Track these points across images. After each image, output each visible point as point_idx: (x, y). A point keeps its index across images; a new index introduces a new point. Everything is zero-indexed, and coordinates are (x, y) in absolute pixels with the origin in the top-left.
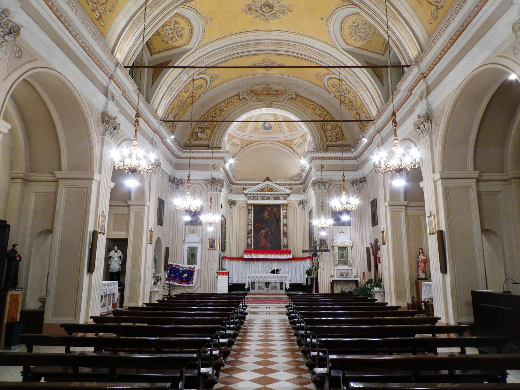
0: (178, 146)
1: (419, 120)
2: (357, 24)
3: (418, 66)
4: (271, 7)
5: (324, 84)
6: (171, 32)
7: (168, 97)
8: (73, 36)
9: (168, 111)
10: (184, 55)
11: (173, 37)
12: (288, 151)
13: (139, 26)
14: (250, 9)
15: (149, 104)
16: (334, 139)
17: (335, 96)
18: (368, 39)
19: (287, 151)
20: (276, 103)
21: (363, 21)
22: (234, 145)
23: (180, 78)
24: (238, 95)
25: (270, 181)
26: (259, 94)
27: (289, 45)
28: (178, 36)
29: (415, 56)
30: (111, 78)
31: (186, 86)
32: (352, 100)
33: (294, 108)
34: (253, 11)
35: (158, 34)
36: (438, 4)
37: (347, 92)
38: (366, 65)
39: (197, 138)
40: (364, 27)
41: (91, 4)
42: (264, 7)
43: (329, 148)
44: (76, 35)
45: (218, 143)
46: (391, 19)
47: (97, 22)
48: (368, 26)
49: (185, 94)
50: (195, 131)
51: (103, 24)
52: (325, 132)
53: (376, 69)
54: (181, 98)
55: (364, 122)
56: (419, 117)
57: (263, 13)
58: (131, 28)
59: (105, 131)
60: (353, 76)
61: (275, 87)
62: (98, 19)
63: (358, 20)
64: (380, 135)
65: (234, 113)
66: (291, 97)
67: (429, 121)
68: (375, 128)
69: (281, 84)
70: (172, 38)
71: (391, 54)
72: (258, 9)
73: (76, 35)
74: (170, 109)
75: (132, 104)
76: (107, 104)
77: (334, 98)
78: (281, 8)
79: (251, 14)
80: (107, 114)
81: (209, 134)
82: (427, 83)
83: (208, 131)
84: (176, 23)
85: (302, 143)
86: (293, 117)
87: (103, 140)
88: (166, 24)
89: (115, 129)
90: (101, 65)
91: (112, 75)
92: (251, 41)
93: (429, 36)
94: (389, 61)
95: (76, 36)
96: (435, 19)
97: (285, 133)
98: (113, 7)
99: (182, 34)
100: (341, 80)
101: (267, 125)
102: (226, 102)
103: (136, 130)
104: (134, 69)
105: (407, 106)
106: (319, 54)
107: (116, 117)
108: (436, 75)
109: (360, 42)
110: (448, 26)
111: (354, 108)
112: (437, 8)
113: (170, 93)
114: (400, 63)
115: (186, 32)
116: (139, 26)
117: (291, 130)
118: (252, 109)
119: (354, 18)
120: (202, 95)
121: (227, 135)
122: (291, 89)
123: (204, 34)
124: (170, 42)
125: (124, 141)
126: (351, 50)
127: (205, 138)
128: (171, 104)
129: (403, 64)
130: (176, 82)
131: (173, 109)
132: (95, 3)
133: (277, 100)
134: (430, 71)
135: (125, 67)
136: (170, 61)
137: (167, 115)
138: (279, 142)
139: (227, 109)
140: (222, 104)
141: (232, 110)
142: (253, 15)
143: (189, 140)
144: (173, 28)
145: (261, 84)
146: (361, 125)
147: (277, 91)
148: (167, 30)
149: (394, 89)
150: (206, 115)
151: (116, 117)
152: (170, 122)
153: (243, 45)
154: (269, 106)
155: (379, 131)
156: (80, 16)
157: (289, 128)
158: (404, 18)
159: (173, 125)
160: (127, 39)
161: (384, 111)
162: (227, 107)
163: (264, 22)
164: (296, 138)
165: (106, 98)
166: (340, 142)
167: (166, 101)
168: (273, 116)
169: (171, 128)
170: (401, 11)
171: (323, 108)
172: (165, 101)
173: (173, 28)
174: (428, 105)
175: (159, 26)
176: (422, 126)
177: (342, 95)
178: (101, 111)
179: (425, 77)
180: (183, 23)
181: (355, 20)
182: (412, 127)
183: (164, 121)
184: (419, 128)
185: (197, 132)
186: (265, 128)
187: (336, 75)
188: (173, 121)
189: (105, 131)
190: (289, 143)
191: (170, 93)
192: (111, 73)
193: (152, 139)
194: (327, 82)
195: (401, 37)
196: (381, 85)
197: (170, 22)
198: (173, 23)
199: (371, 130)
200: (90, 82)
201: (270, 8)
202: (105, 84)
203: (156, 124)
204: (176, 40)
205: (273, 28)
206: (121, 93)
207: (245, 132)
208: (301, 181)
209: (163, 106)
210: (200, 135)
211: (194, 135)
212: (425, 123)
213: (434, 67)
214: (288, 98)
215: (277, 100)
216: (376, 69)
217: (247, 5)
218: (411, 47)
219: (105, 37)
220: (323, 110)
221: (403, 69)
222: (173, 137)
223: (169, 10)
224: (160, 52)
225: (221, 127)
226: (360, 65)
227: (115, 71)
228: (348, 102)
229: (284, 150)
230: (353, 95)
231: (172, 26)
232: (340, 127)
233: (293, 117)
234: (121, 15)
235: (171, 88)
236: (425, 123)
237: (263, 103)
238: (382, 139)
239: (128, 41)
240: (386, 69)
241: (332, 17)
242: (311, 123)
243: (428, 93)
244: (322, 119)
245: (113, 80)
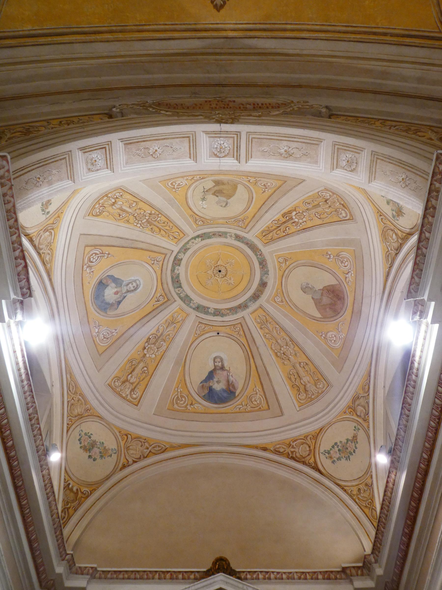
12: (300, 478)
19: (297, 479)
25: (231, 572)
85: (355, 439)
138: (265, 449)
190: (302, 451)
207: (137, 403)
208: (379, 571)
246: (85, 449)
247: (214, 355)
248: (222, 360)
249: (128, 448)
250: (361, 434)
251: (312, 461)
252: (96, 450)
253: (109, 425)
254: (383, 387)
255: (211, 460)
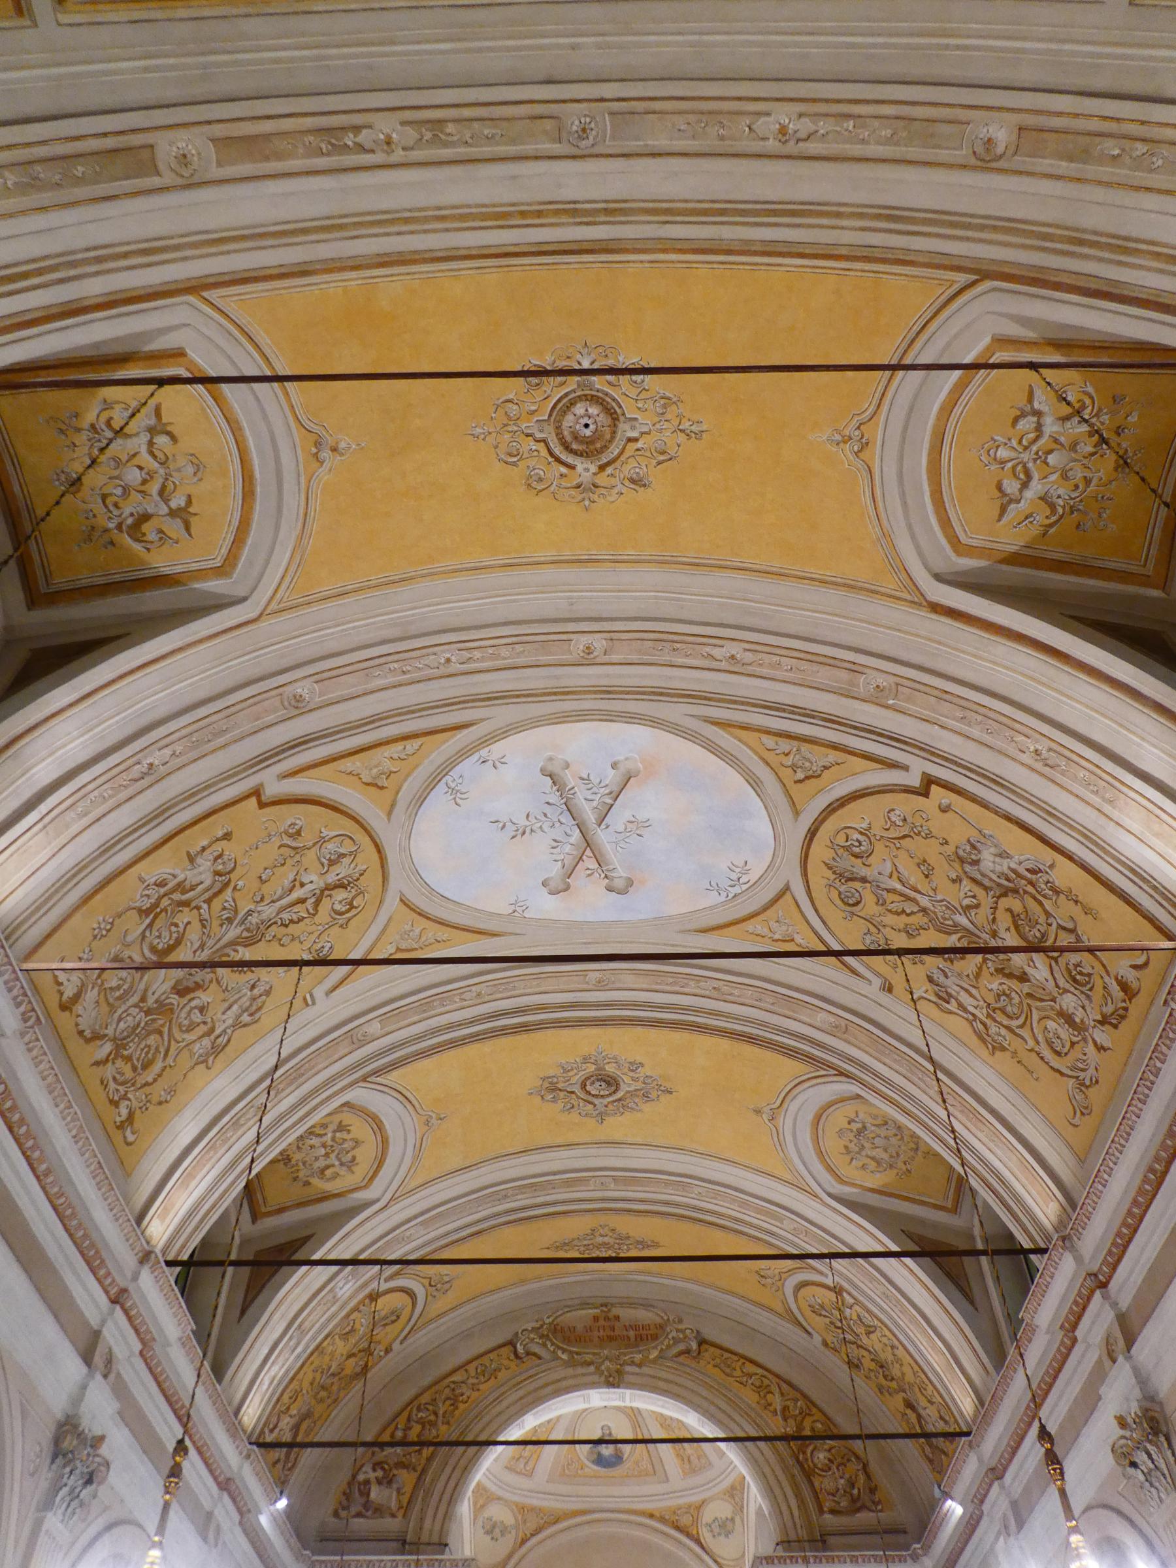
0: (293, 1540)
1: (1127, 1434)
2: (860, 1125)
3: (1073, 1249)
4: (611, 1082)
5: (784, 1302)
6: (323, 1151)
7: (286, 1354)
8: (38, 1177)
9: (277, 1408)
10: (352, 1218)
11: (327, 1167)
13: (232, 1141)
14: (554, 1088)
15: (220, 1381)
16: (844, 1504)
17: (825, 1344)
18: (900, 1165)
20: (637, 1370)
21: (875, 1117)
22: (492, 1530)
23: (331, 1290)
24: (511, 1343)
26: (579, 1340)
27: (667, 1183)
28: (342, 1164)
29: (1054, 1219)
30: (118, 1299)
31: (348, 1315)
32: (882, 1356)
33: (695, 1387)
34: (562, 1094)
35: (284, 1158)
36: (1082, 1075)
37: (861, 1330)
38: (913, 1247)
39: (367, 1505)
40: (883, 1132)
41: (112, 1086)
42: (593, 1083)
43: (832, 1540)
44: (48, 1172)
45: (437, 1527)
46: (959, 1116)
47: (117, 1137)
48: (894, 1131)
49: (340, 1344)
50: (361, 1477)
51: (131, 1138)
52: (808, 1475)
53: (944, 1260)
54: (327, 1358)
55: (942, 1440)
56: (1122, 1422)
57: (590, 1098)
58: (212, 1147)
59: (55, 1488)
60: (873, 1279)
61: (628, 1315)
62: (121, 1127)
63: (861, 1115)
64: (1002, 1487)
65: (498, 1409)
66: (681, 1347)
67: (1162, 1439)
68: (980, 1460)
69: (647, 1305)
70: (322, 1171)
71: (980, 1210)
72: (577, 1089)
73: (48, 1172)
74: (286, 1397)
75: (165, 1385)
76: (84, 1387)
77: (823, 1348)
78: (639, 1085)
79: (555, 1100)
80: (76, 1426)
81: (408, 1489)
82: (1114, 1305)
83: (406, 1478)
84: (341, 1128)
85: (732, 1520)
86: (695, 1423)
87: (38, 1524)
88: (310, 1132)
89: (89, 1481)
90: (94, 1258)
91: (124, 1291)
92: (554, 1174)
93: (1082, 1161)
94: (977, 1231)
95: (46, 1175)
96: (1083, 1114)
97: (669, 1482)
98: (172, 1091)
99: (354, 1158)
100: (838, 1290)
101: (607, 1450)
102: (471, 1368)
103: (166, 1506)
104: (192, 1271)
105: (1068, 1383)
106: (760, 1210)
107: (102, 1438)
108: (1138, 1278)
109: (878, 1175)
110: (1129, 1134)
111: (894, 1385)
112: (1083, 1084)
113: (292, 1343)
114: (1011, 1236)
115: (366, 1155)
116: (232, 1141)
117: (691, 1468)
118: (558, 1393)
119: (849, 1109)
120: (396, 1346)
121: (469, 1493)
122: (681, 1321)
123: (417, 1157)
124: (315, 1181)
125: (109, 1527)
126: (860, 1200)
127: (394, 1505)
128: (293, 1379)
129: (1027, 1244)
130: (319, 1304)
131: (294, 1398)
132: (122, 1084)
133: (638, 1357)
134: (1114, 1267)
135: (169, 1264)
136: (305, 1240)
137: (274, 1420)
138: (651, 1516)
139: (475, 1394)
140: (456, 1377)
141: (491, 1398)
142: (560, 1105)
143: (336, 1514)
144: (330, 1143)
145: (585, 1305)
146: (927, 1449)
147: (635, 1327)
148: (312, 1147)
149: (1015, 1322)
150: (405, 1414)
151: (102, 1438)
152: (277, 1448)
153: (532, 1185)
154: (614, 1380)
155: (996, 1473)
156: (73, 1120)
157: (684, 1459)
158: (993, 1111)
159: (288, 1456)
160: (191, 1176)
161: (996, 1399)
162: (474, 1388)
163: (591, 1123)
164: (712, 1499)
165: (84, 1369)
166: (864, 1518)
167: (276, 1371)
168: (628, 1416)
169: (279, 1466)
170: (981, 1093)
171: (790, 1384)
172: (276, 1368)
173: (330, 1143)
174: (1142, 1379)
175: (292, 1138)
176: (1141, 1457)
177: (848, 1336)
178: (60, 1416)
179: (1104, 1285)
180: (360, 1129)
181: (853, 1116)
182: (1107, 1461)
183: (260, 1445)
184: (1134, 1465)
185: (367, 1482)
186: (600, 1461)
187: (821, 1273)
188: (291, 1445)
189: (55, 1488)
190: (685, 1520)
191: (292, 1343)
192: (122, 1284)
193: (209, 1515)
194: (796, 1297)
195: (997, 1164)
196: (970, 1308)
197: (324, 1126)
198: (332, 1127)
199: (969, 1469)
200: (50, 1319)
201: (609, 1084)
202: (94, 1322)
203: (230, 1452)
204: (336, 1176)
205: (618, 1137)
206: (137, 1346)
207: (530, 1474)
209: (265, 1387)
210: (375, 1493)
211: (354, 1495)
212: (1149, 1446)
213: (1124, 1252)
214: (675, 1350)
215: (638, 1357)
216: (941, 1256)
217: (544, 1079)
218: (1034, 1192)
219: (128, 1175)
220: (793, 1394)
221: (1027, 1261)
222: (282, 1503)
223: (324, 1096)
224: (281, 1210)
225: (452, 1462)
226: (895, 1248)
227: (135, 1277)
228: (873, 1366)
229: (668, 1546)
230: (884, 1340)
231: (330, 1135)
232: (858, 1457)
233: (695, 1423)
234: (188, 1113)
235: (300, 1326)
236: (1149, 1446)
237: (592, 1368)
238: (1014, 1505)
239: (193, 1184)
240: (980, 1261)
241: (785, 1105)
242: (761, 1444)
243: (1130, 1341)
244: (790, 1429)
245: (123, 1307)
246: (487, 1533)
247: (603, 1423)
248: (609, 1428)
249: (525, 1522)
250: (738, 1519)
251: (695, 1532)
252: (497, 1531)
253: (506, 1502)
254: (1146, 477)
255: (602, 1529)
